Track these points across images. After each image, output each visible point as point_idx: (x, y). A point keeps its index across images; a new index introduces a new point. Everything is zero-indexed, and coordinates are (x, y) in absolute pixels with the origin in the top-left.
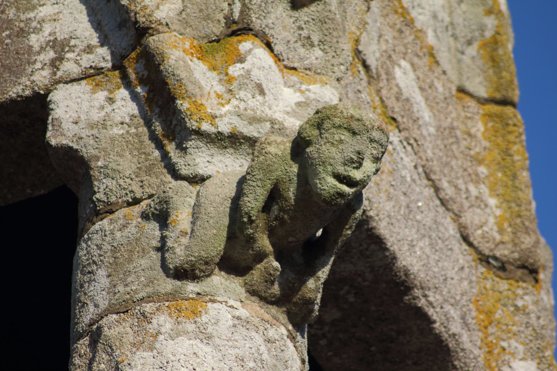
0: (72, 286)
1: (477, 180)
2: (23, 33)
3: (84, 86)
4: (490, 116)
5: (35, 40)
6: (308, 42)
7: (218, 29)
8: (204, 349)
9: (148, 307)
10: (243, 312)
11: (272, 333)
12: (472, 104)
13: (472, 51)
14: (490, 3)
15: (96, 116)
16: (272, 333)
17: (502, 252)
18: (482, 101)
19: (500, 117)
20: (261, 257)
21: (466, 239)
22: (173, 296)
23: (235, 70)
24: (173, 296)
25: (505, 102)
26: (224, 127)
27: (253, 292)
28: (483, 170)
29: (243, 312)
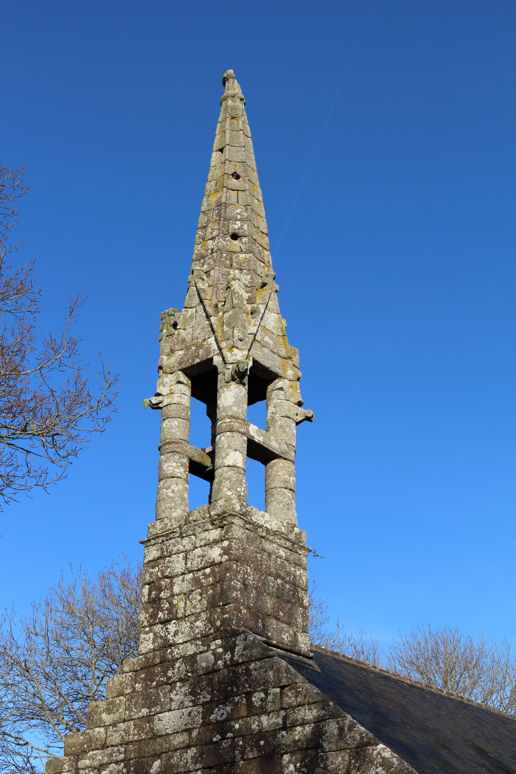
0: (277, 303)
1: (281, 347)
2: (210, 349)
3: (217, 356)
4: (282, 338)
5: (212, 350)
6: (244, 345)
7: (231, 347)
8: (230, 392)
9: (224, 387)
10: (235, 386)
11: (240, 388)
12: (280, 337)
13: (279, 330)
14: (1, 687)
15: (218, 360)
16: (240, 388)
17: (286, 356)
18: (281, 336)
19: (284, 338)
20: (236, 379)
21: (280, 357)
22: (226, 386)
23: (233, 353)
24: (226, 386)
25: (284, 336)
26: (231, 362)
27: (236, 383)
28: (282, 346)
29: (235, 386)
